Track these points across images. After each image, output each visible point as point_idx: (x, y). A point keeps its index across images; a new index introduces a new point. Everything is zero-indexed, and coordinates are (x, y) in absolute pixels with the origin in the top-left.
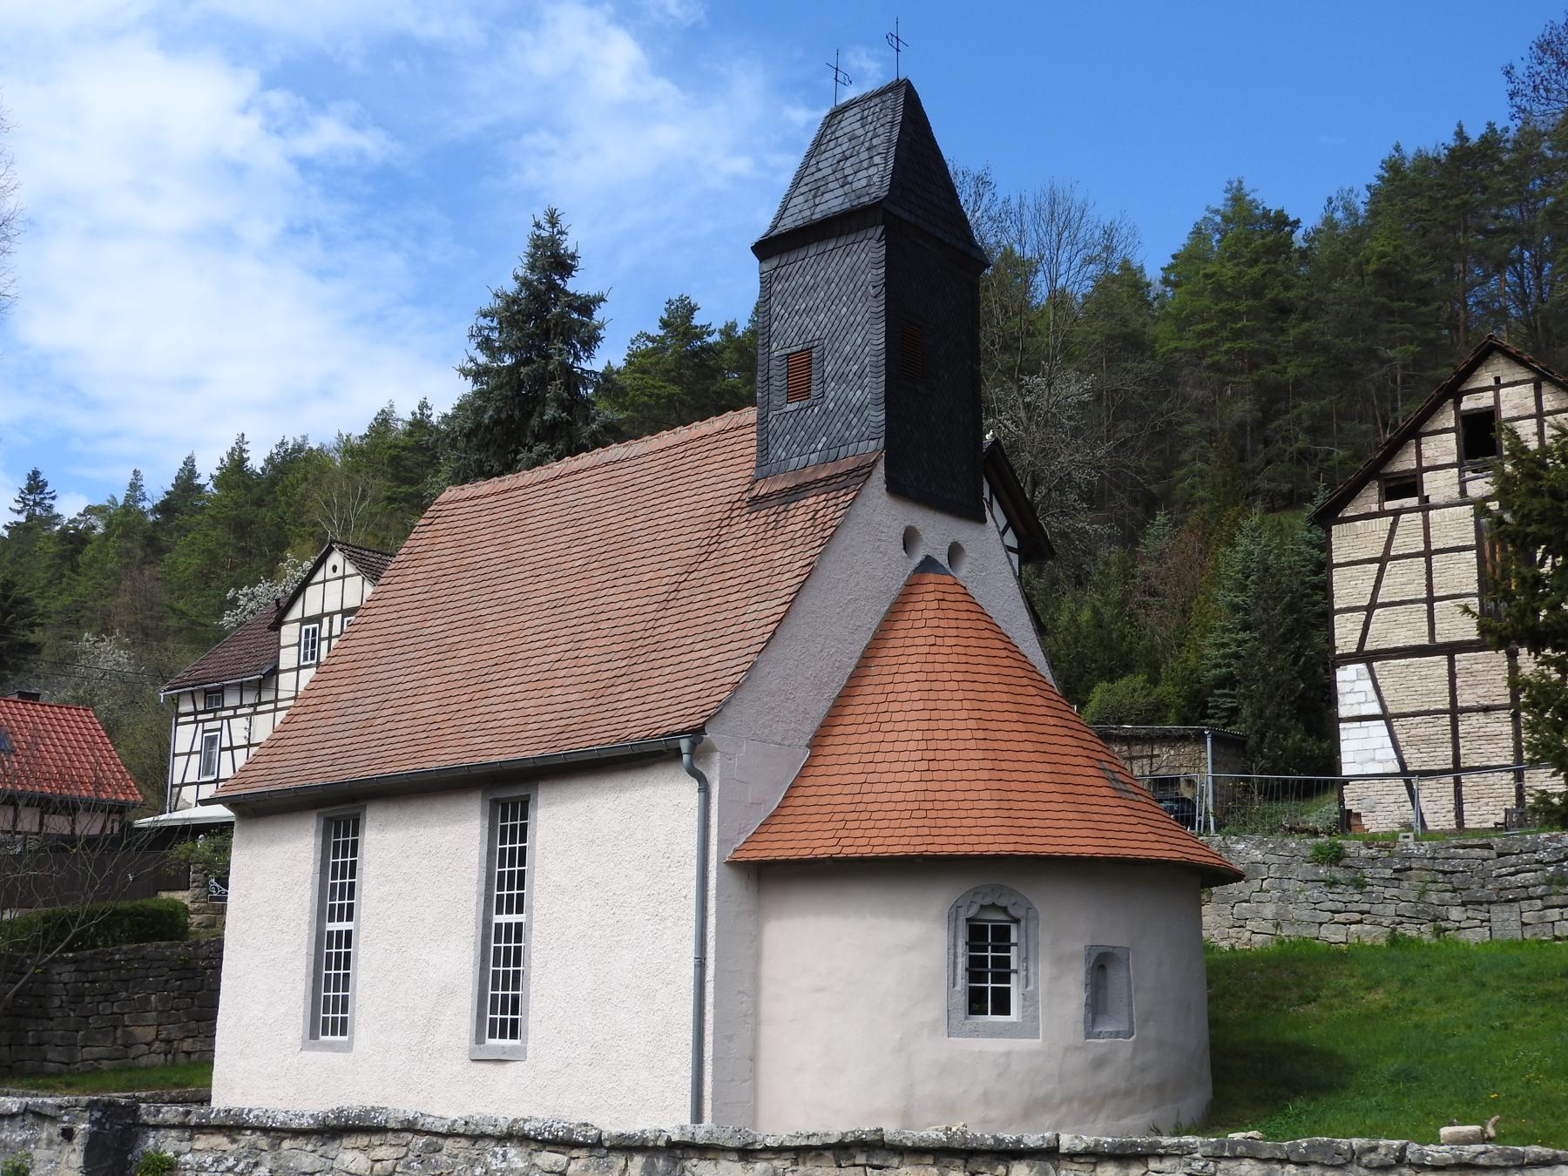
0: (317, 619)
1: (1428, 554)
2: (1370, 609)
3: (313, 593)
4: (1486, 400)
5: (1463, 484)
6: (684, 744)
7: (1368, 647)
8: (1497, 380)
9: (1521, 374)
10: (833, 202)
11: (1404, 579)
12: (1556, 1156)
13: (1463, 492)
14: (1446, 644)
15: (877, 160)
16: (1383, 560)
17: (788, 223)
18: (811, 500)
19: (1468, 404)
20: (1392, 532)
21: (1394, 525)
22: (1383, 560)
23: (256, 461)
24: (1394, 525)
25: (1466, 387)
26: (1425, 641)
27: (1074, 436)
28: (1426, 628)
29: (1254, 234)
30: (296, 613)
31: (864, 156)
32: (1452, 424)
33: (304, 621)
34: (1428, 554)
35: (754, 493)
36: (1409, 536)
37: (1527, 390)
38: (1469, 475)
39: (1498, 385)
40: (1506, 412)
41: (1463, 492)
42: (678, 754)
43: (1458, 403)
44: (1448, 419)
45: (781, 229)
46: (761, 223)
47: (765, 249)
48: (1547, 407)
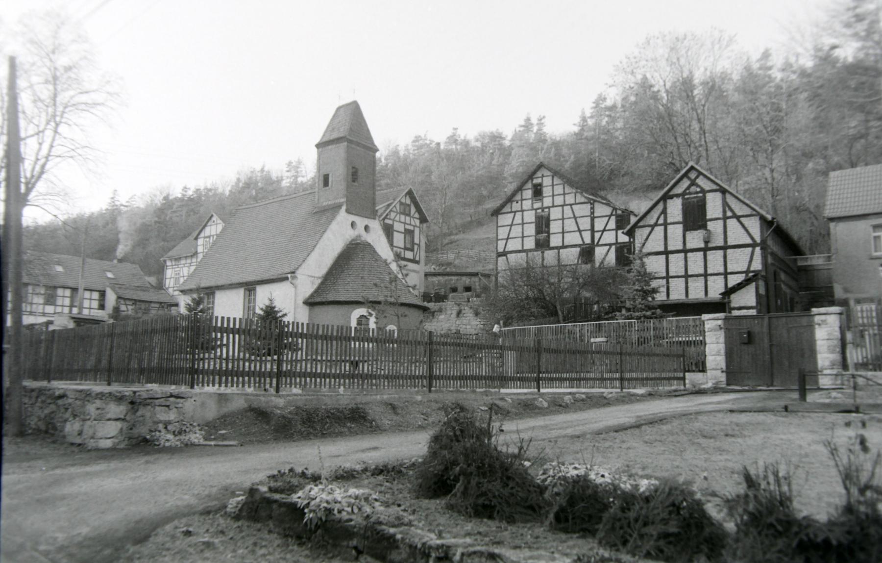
0: (209, 237)
1: (523, 224)
2: (507, 239)
3: (207, 229)
4: (539, 181)
9: (549, 173)
10: (335, 135)
11: (516, 231)
12: (602, 397)
17: (325, 139)
19: (535, 181)
20: (650, 233)
23: (171, 198)
26: (520, 248)
28: (702, 264)
29: (496, 138)
30: (202, 235)
33: (205, 237)
34: (523, 224)
37: (550, 178)
39: (543, 176)
45: (21, 115)
46: (318, 139)
47: (318, 146)
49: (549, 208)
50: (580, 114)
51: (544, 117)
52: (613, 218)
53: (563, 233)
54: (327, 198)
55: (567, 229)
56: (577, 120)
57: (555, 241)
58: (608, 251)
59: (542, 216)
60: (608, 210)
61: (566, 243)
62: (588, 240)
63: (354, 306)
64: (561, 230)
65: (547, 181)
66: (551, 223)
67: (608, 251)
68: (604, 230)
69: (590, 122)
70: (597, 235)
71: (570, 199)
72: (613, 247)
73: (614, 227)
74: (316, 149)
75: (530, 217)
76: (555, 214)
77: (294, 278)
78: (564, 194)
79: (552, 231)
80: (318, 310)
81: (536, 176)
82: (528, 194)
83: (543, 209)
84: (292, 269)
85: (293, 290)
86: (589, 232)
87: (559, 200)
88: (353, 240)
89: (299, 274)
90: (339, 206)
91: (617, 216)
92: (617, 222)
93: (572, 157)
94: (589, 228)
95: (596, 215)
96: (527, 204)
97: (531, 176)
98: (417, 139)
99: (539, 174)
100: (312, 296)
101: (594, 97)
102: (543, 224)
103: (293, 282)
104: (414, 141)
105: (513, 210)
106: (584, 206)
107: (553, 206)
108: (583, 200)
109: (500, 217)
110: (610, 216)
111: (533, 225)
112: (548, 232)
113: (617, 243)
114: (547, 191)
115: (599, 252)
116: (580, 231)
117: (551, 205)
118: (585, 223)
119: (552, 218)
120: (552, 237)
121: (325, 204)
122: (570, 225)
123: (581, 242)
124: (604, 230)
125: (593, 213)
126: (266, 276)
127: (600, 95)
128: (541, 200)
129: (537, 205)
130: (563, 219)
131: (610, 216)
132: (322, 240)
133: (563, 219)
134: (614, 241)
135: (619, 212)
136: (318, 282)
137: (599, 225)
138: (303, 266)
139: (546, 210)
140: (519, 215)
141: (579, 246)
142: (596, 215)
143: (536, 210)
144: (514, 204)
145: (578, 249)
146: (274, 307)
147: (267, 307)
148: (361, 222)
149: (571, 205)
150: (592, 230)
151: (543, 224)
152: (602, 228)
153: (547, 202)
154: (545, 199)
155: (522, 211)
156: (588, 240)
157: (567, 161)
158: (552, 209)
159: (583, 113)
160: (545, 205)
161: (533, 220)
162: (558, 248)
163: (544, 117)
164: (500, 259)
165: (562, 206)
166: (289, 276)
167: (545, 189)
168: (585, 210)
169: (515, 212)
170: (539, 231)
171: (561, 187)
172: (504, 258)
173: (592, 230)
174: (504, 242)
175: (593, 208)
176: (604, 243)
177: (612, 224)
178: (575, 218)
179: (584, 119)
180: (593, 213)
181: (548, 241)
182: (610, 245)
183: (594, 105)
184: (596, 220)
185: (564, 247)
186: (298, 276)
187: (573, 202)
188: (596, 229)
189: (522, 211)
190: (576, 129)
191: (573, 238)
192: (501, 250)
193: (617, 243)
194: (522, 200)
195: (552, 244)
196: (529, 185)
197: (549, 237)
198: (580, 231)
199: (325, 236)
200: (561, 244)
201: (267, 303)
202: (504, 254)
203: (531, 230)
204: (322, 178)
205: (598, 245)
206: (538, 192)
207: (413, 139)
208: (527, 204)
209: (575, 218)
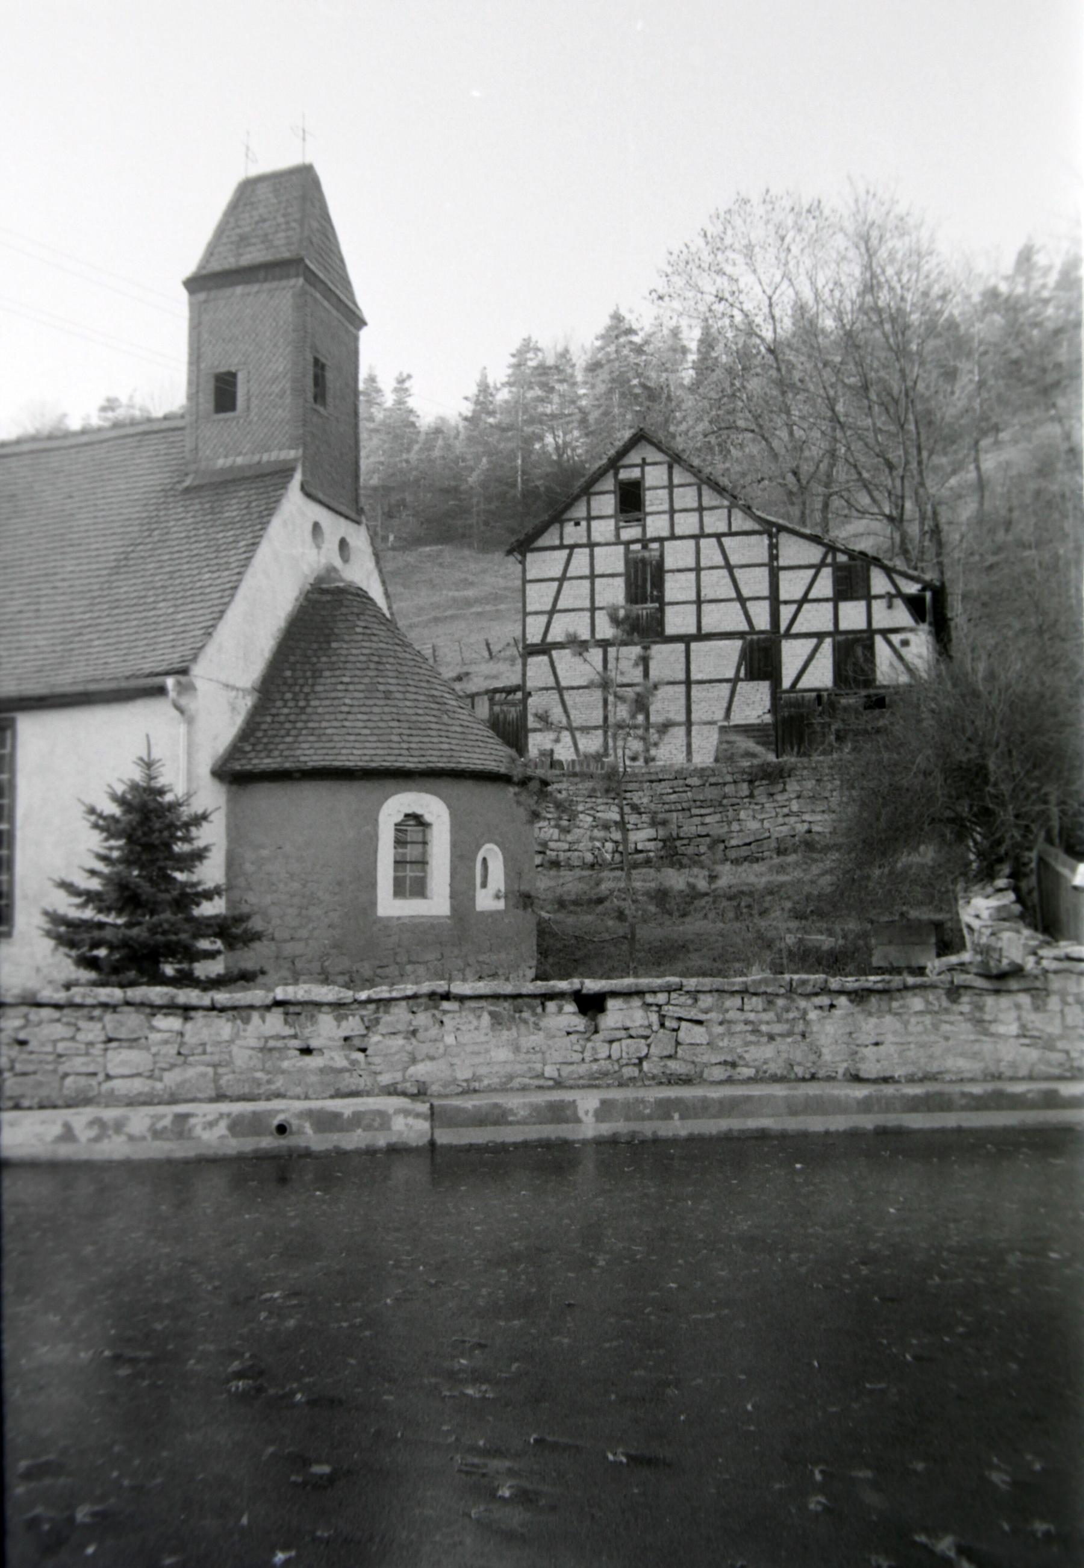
1: (592, 577)
4: (636, 473)
5: (618, 529)
6: (170, 682)
7: (549, 639)
8: (644, 459)
9: (660, 457)
10: (254, 255)
11: (575, 594)
13: (618, 535)
14: (603, 640)
15: (294, 225)
16: (562, 579)
17: (216, 266)
18: (242, 493)
19: (624, 475)
21: (570, 556)
22: (562, 579)
24: (570, 556)
25: (622, 463)
27: (734, 395)
31: (281, 220)
32: (612, 488)
34: (592, 577)
35: (186, 484)
36: (580, 562)
37: (664, 469)
38: (622, 524)
39: (644, 463)
40: (649, 482)
41: (618, 535)
42: (161, 691)
43: (616, 474)
44: (608, 483)
46: (190, 266)
47: (194, 284)
48: (676, 481)
49: (661, 540)
50: (477, 377)
51: (409, 377)
52: (827, 573)
53: (699, 602)
54: (229, 448)
55: (707, 593)
56: (473, 390)
57: (678, 621)
58: (816, 650)
59: (643, 561)
60: (813, 553)
61: (705, 629)
62: (762, 621)
63: (390, 784)
64: (693, 596)
65: (655, 476)
66: (668, 577)
67: (816, 650)
68: (805, 600)
69: (503, 395)
70: (786, 613)
71: (715, 522)
72: (828, 642)
73: (829, 592)
74: (184, 294)
75: (611, 560)
76: (677, 555)
77: (187, 688)
78: (701, 509)
79: (669, 596)
80: (267, 800)
81: (626, 461)
82: (606, 504)
83: (645, 542)
84: (174, 659)
85: (182, 729)
86: (766, 604)
87: (687, 523)
88: (319, 579)
89: (198, 670)
90: (284, 473)
91: (837, 568)
92: (837, 582)
93: (484, 460)
94: (765, 592)
95: (782, 562)
96: (603, 530)
97: (614, 464)
98: (110, 405)
99: (634, 457)
100: (235, 750)
101: (515, 345)
102: (645, 578)
103: (183, 701)
104: (104, 409)
105: (567, 541)
106: (754, 539)
107: (673, 537)
108: (750, 525)
109: (530, 557)
110: (818, 568)
111: (620, 582)
112: (660, 599)
113: (836, 632)
114: (654, 500)
115: (792, 654)
116: (742, 600)
117: (665, 533)
118: (755, 582)
119: (669, 564)
120: (669, 611)
121: (221, 462)
122: (717, 584)
123: (744, 627)
124: (805, 600)
125: (774, 557)
126: (63, 681)
127: (527, 341)
128: (641, 521)
129: (631, 532)
130: (698, 569)
131: (818, 568)
132: (250, 571)
133: (698, 569)
134: (830, 627)
135: (842, 558)
136: (246, 703)
137: (791, 586)
138: (210, 650)
139: (655, 546)
140: (581, 557)
141: (740, 635)
142: (782, 562)
143: (627, 544)
144: (569, 528)
145: (738, 644)
146: (161, 792)
147: (134, 787)
148: (335, 527)
149: (718, 536)
150: (775, 600)
151: (645, 578)
152: (798, 595)
153: (657, 526)
154: (649, 520)
155: (591, 545)
156: (762, 621)
157: (472, 469)
158: (666, 544)
159: (484, 376)
160: (650, 534)
161: (620, 567)
162: (686, 640)
163: (409, 377)
164: (533, 660)
165: (696, 537)
166: (170, 682)
167: (649, 496)
168: (757, 548)
169: (572, 547)
170: (635, 594)
171: (692, 492)
172: (545, 658)
173: (775, 600)
174: (544, 619)
175: (773, 546)
176: (804, 630)
177: (825, 586)
178: (729, 567)
179: (484, 389)
180: (774, 557)
181: (661, 623)
182: (820, 636)
183: (514, 361)
184: (783, 575)
185: (701, 636)
186: (199, 684)
187: (723, 528)
188: (783, 595)
189: (591, 545)
190: (467, 409)
191: (725, 617)
192: (534, 636)
193: (836, 632)
194: (589, 518)
195: (670, 630)
196: (608, 483)
197: (661, 610)
198: (742, 600)
199: (264, 552)
200: (693, 630)
201: (137, 775)
202: (544, 648)
203: (613, 593)
204: (209, 387)
205: (788, 635)
206: (631, 500)
207: (102, 402)
208: (603, 530)
209: (729, 567)
